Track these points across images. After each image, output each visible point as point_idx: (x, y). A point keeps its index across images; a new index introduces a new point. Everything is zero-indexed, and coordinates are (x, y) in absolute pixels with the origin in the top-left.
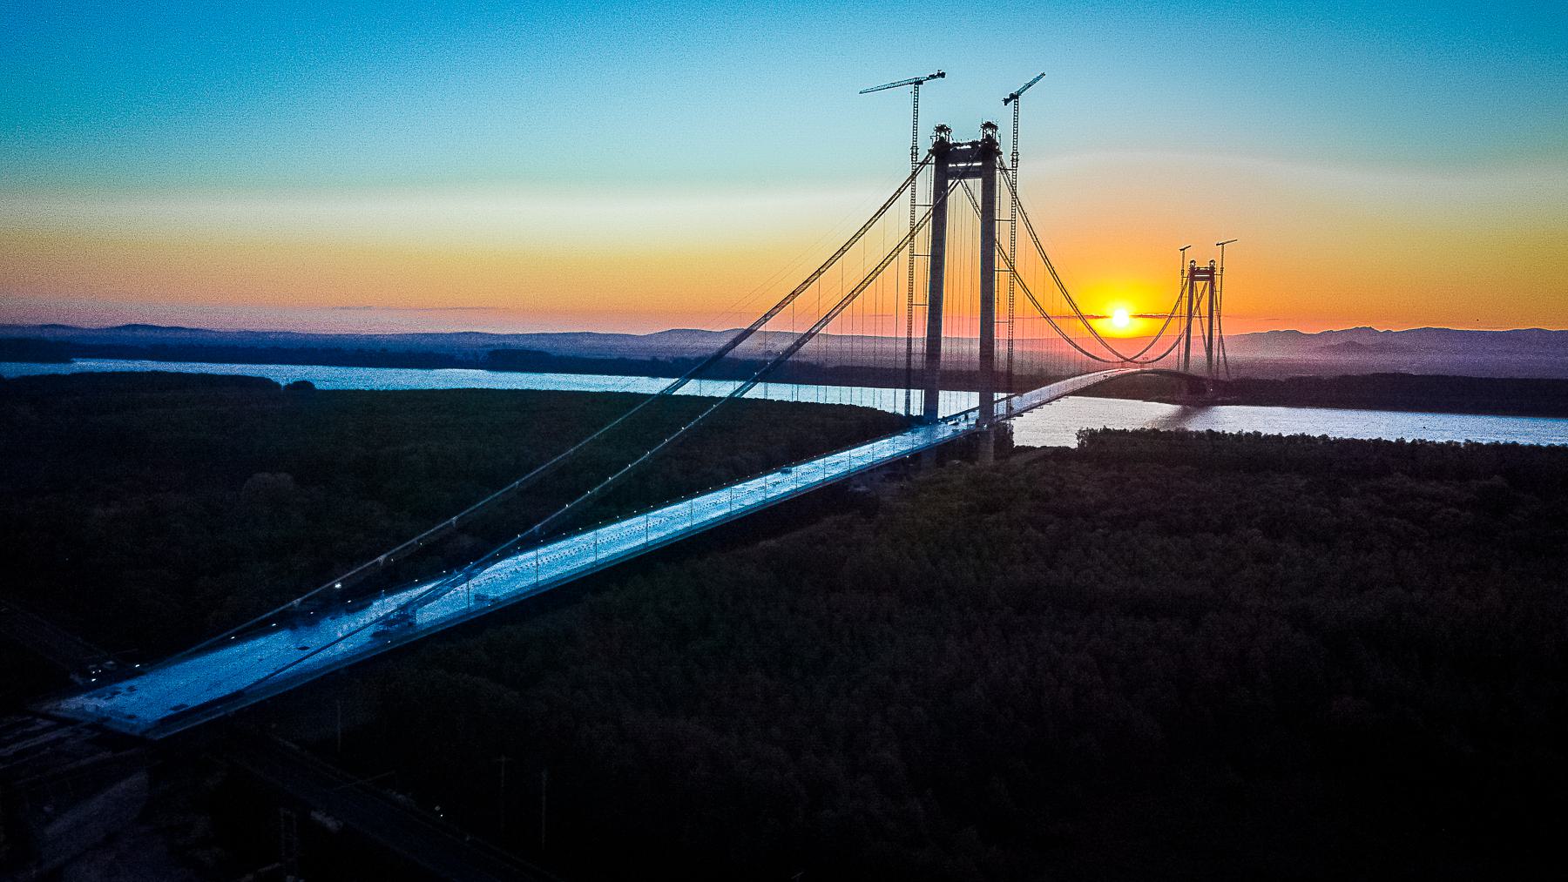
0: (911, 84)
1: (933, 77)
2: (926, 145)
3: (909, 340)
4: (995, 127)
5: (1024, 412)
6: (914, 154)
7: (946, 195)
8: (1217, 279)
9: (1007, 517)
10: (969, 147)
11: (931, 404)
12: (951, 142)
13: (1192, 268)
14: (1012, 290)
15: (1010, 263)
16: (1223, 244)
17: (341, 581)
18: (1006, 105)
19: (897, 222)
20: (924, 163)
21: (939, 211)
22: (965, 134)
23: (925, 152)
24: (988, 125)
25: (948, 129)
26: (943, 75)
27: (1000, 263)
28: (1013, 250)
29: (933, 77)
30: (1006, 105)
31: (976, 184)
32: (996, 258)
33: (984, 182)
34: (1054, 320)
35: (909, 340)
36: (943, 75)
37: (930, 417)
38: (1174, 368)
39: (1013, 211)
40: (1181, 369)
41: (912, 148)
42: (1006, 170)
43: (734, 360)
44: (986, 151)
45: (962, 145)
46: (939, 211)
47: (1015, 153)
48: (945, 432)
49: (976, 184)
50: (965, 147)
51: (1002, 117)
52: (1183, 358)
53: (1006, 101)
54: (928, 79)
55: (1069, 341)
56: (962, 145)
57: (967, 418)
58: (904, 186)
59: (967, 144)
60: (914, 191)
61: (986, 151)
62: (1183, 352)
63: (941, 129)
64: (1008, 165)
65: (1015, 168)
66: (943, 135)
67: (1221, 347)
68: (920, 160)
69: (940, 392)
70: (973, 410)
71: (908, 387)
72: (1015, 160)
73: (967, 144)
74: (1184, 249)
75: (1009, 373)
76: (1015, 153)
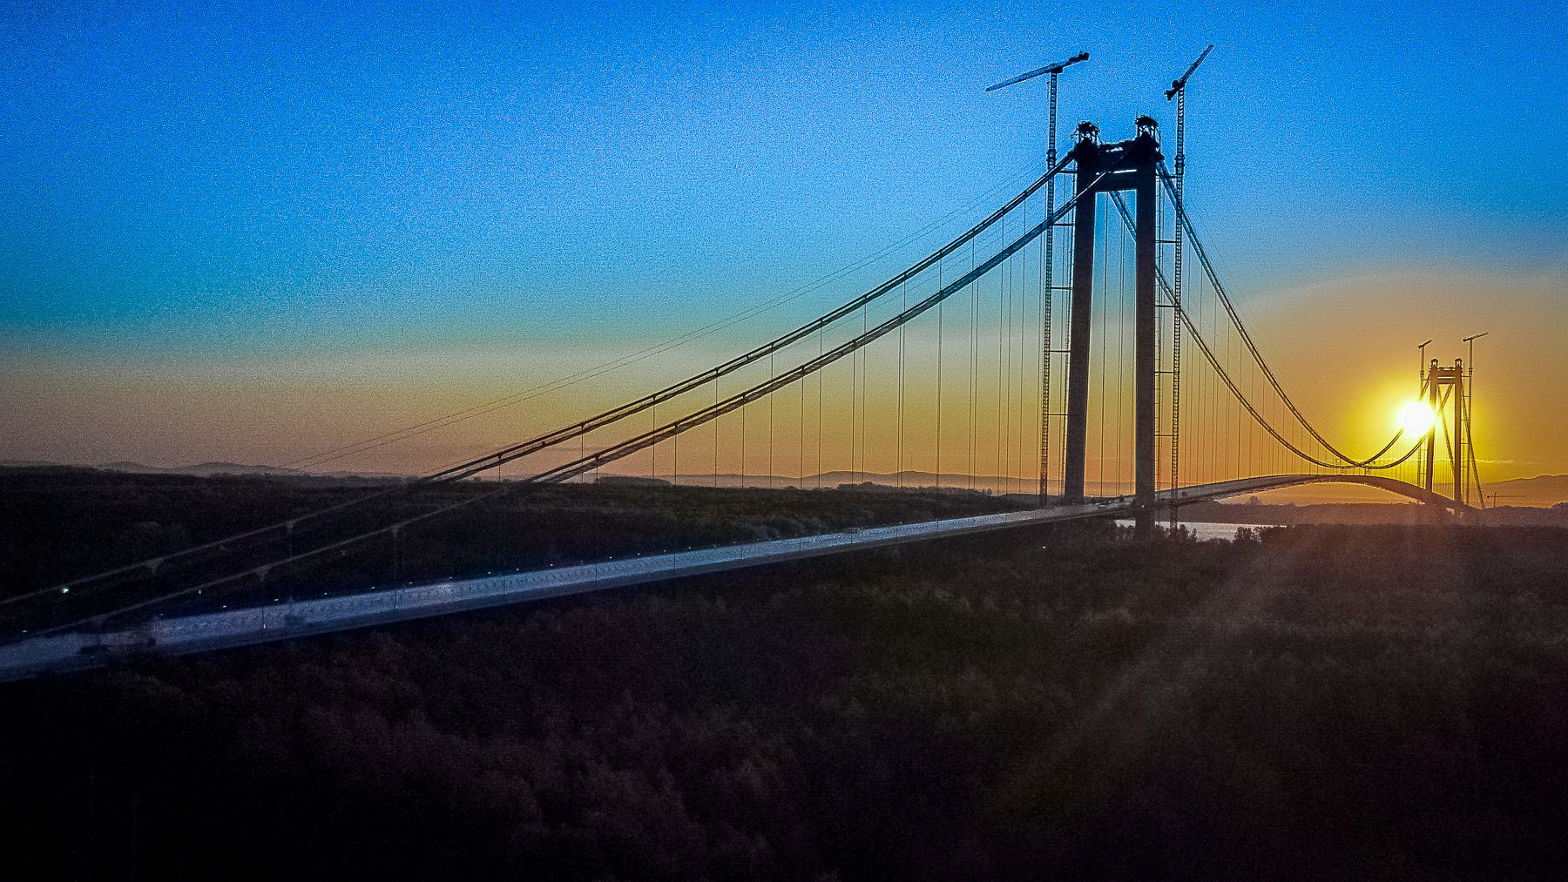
0: (1047, 72)
1: (1073, 60)
2: (1068, 140)
4: (1155, 124)
6: (1051, 159)
8: (1465, 381)
9: (402, 499)
10: (1121, 149)
13: (1434, 368)
16: (1471, 339)
17: (70, 588)
18: (1169, 99)
19: (1034, 209)
21: (1085, 207)
22: (1114, 134)
24: (1145, 121)
25: (1093, 127)
26: (1084, 57)
27: (1160, 297)
28: (1178, 287)
29: (1073, 60)
30: (1169, 99)
31: (1129, 196)
32: (1157, 288)
33: (1138, 192)
34: (1045, 233)
36: (1084, 57)
39: (1178, 230)
41: (1048, 153)
42: (1168, 177)
44: (1143, 153)
45: (1113, 147)
46: (1085, 207)
49: (1129, 196)
50: (1116, 149)
51: (1166, 114)
52: (1424, 466)
53: (1170, 94)
54: (1068, 64)
56: (1113, 147)
58: (1040, 228)
59: (1117, 146)
61: (1143, 153)
62: (1424, 458)
63: (1085, 128)
64: (1172, 171)
65: (1179, 175)
67: (1471, 463)
72: (1180, 165)
73: (1117, 146)
74: (1423, 346)
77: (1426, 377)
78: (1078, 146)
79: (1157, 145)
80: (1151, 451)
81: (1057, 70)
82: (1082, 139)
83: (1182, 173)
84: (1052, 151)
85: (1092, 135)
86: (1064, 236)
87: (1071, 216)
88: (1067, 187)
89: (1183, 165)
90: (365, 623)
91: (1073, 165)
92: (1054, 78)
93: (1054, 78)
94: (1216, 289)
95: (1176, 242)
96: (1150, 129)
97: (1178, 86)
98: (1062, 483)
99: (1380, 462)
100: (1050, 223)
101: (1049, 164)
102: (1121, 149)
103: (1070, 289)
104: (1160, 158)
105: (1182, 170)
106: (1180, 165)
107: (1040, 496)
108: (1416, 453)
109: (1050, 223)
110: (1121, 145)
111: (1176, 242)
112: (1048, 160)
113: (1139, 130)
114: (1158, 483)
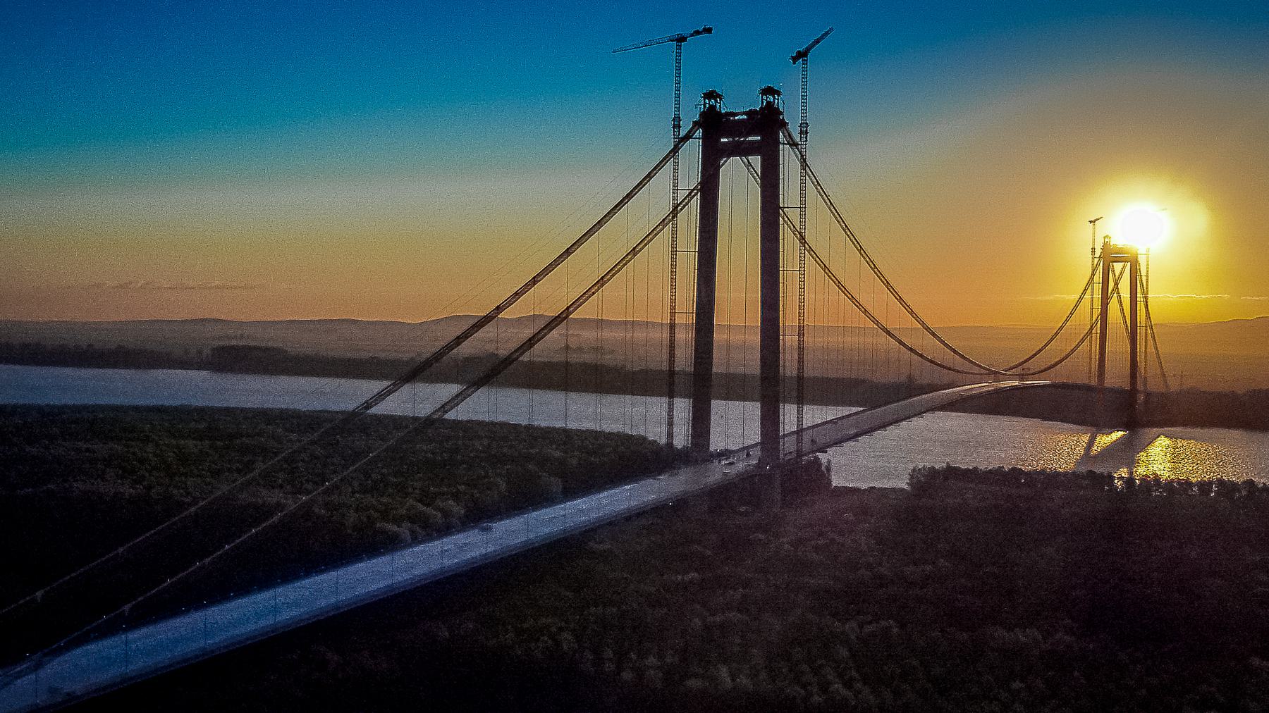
0: (673, 41)
1: (698, 33)
2: (690, 116)
3: (672, 326)
4: (779, 93)
5: (828, 447)
6: (677, 126)
7: (719, 167)
10: (745, 117)
11: (701, 421)
12: (723, 111)
14: (804, 188)
15: (800, 152)
18: (794, 63)
19: (658, 198)
20: (688, 137)
21: (708, 189)
23: (688, 124)
24: (769, 91)
26: (709, 31)
29: (698, 33)
30: (794, 63)
32: (781, 227)
35: (672, 326)
36: (709, 31)
37: (699, 452)
38: (1081, 379)
40: (1094, 382)
41: (674, 120)
43: (386, 378)
46: (708, 189)
47: (804, 125)
48: (717, 473)
53: (795, 59)
54: (692, 35)
55: (888, 333)
57: (748, 455)
58: (663, 223)
60: (674, 232)
63: (710, 95)
66: (771, 98)
68: (683, 133)
69: (713, 402)
70: (753, 446)
71: (671, 395)
72: (804, 133)
75: (800, 379)
76: (804, 125)
77: (1097, 255)
78: (703, 114)
79: (782, 113)
80: (838, 381)
81: (681, 39)
82: (707, 106)
83: (806, 141)
84: (677, 119)
85: (716, 101)
86: (691, 214)
87: (696, 202)
88: (693, 151)
89: (807, 133)
90: (512, 551)
91: (699, 133)
92: (679, 47)
93: (679, 47)
94: (846, 233)
95: (800, 208)
96: (774, 98)
97: (802, 55)
98: (693, 328)
99: (1035, 364)
100: (675, 212)
101: (674, 131)
102: (745, 117)
103: (699, 138)
104: (783, 124)
105: (806, 138)
106: (804, 133)
107: (802, 404)
108: (1086, 343)
109: (675, 212)
110: (745, 113)
111: (800, 208)
112: (674, 128)
113: (762, 99)
114: (1022, 377)
